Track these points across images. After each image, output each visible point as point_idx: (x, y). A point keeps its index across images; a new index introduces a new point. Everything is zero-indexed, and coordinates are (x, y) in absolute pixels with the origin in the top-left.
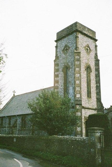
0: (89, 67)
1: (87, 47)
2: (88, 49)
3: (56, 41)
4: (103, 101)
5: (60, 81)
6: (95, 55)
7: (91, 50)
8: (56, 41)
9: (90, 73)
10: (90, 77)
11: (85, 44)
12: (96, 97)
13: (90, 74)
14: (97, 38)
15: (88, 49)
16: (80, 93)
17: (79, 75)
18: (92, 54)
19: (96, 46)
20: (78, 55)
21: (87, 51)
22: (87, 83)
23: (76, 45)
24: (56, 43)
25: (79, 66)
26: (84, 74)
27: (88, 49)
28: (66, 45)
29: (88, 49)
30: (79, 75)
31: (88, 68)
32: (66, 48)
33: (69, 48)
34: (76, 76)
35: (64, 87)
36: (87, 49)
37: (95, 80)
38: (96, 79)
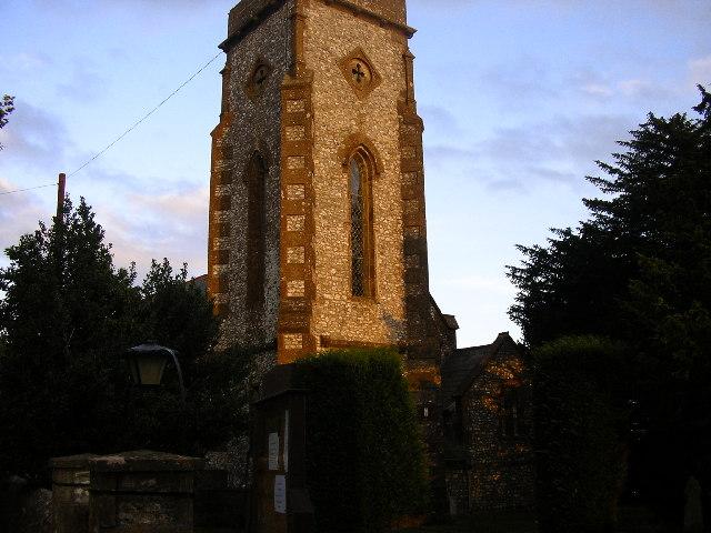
0: (365, 155)
1: (357, 62)
2: (359, 72)
3: (225, 46)
4: (67, 189)
5: (235, 225)
6: (403, 100)
7: (378, 76)
8: (225, 46)
9: (370, 179)
10: (371, 198)
11: (340, 49)
12: (402, 295)
13: (371, 185)
14: (410, 23)
15: (364, 69)
16: (306, 271)
17: (299, 191)
18: (387, 93)
19: (407, 59)
20: (295, 100)
21: (359, 80)
22: (349, 227)
23: (294, 56)
24: (224, 56)
25: (306, 147)
26: (332, 187)
27: (359, 72)
28: (258, 61)
29: (364, 69)
30: (299, 191)
31: (359, 157)
32: (259, 74)
33: (270, 69)
34: (285, 194)
35: (250, 254)
36: (354, 72)
37: (398, 211)
38: (404, 207)
